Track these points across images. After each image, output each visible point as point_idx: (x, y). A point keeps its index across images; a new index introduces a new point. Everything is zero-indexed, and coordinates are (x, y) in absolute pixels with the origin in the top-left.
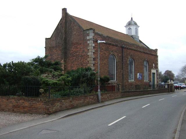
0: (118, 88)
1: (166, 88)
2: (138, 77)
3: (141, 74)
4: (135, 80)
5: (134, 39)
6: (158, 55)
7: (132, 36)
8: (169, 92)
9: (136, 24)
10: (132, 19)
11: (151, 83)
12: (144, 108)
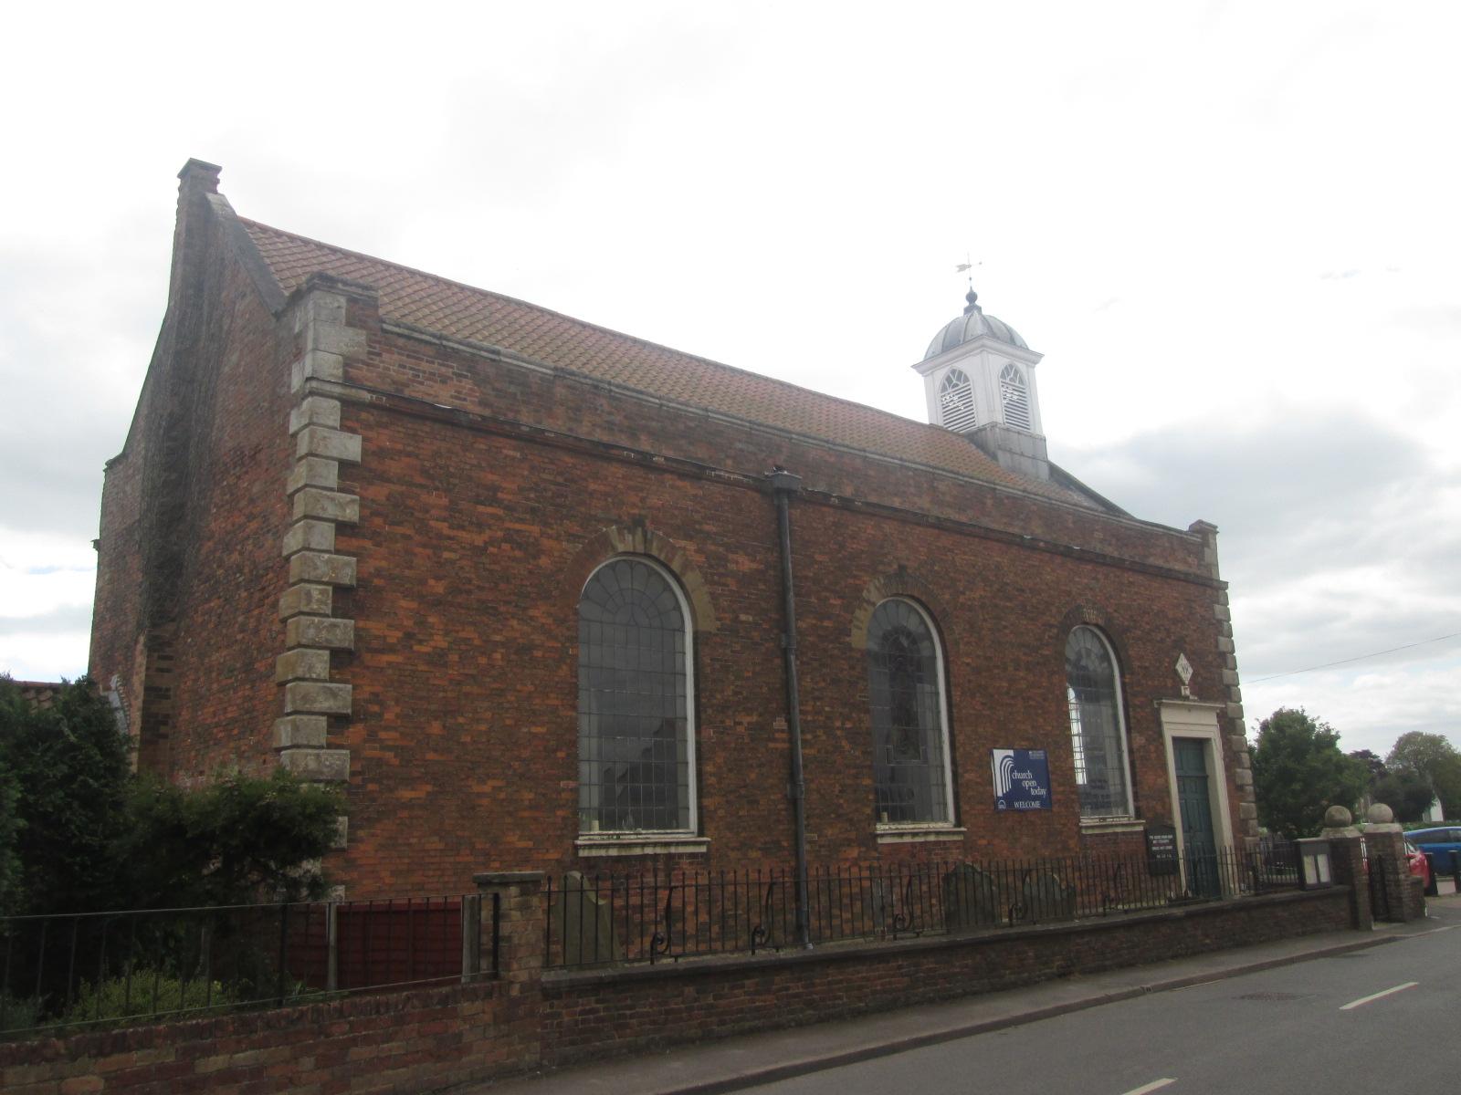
0: (486, 940)
1: (1319, 885)
2: (1001, 787)
3: (1036, 755)
4: (959, 823)
5: (994, 457)
6: (1222, 578)
7: (976, 433)
8: (1355, 924)
9: (1004, 337)
10: (978, 303)
11: (1166, 838)
12: (1159, 1077)
